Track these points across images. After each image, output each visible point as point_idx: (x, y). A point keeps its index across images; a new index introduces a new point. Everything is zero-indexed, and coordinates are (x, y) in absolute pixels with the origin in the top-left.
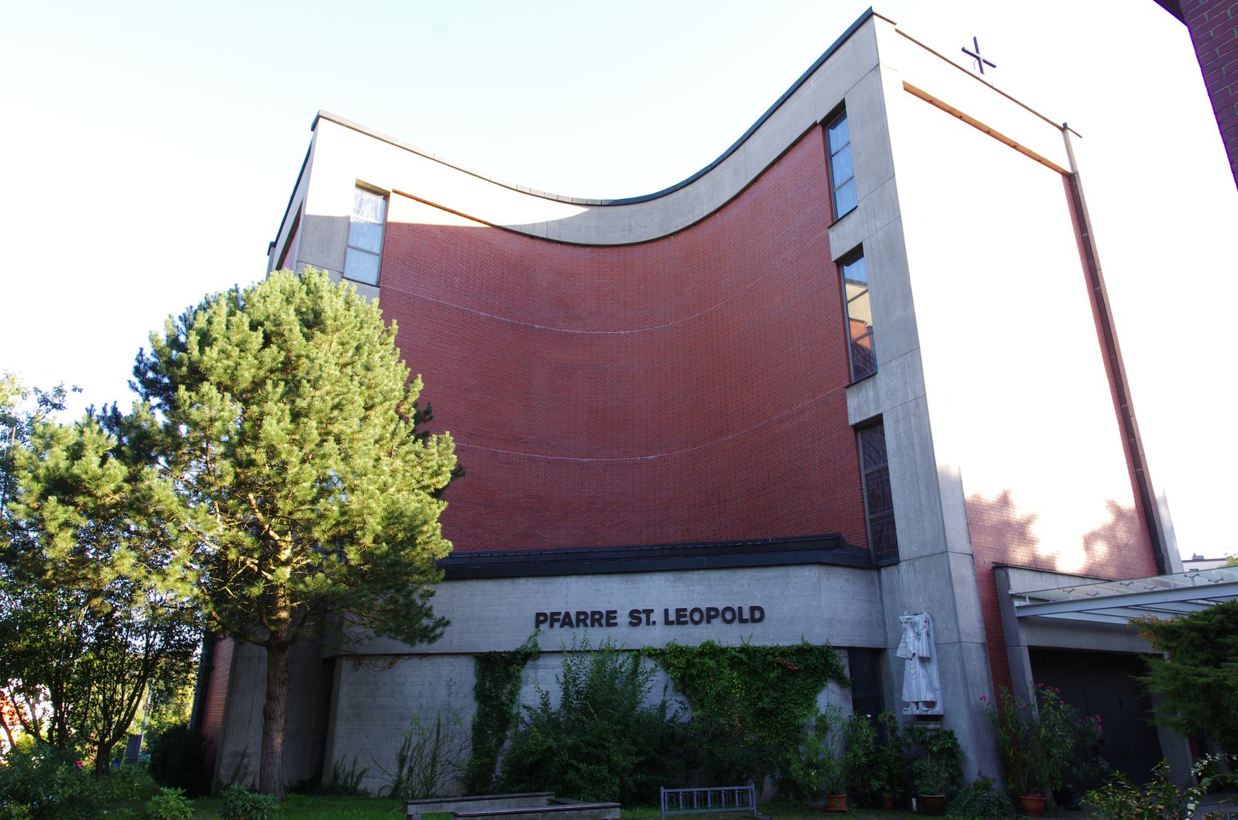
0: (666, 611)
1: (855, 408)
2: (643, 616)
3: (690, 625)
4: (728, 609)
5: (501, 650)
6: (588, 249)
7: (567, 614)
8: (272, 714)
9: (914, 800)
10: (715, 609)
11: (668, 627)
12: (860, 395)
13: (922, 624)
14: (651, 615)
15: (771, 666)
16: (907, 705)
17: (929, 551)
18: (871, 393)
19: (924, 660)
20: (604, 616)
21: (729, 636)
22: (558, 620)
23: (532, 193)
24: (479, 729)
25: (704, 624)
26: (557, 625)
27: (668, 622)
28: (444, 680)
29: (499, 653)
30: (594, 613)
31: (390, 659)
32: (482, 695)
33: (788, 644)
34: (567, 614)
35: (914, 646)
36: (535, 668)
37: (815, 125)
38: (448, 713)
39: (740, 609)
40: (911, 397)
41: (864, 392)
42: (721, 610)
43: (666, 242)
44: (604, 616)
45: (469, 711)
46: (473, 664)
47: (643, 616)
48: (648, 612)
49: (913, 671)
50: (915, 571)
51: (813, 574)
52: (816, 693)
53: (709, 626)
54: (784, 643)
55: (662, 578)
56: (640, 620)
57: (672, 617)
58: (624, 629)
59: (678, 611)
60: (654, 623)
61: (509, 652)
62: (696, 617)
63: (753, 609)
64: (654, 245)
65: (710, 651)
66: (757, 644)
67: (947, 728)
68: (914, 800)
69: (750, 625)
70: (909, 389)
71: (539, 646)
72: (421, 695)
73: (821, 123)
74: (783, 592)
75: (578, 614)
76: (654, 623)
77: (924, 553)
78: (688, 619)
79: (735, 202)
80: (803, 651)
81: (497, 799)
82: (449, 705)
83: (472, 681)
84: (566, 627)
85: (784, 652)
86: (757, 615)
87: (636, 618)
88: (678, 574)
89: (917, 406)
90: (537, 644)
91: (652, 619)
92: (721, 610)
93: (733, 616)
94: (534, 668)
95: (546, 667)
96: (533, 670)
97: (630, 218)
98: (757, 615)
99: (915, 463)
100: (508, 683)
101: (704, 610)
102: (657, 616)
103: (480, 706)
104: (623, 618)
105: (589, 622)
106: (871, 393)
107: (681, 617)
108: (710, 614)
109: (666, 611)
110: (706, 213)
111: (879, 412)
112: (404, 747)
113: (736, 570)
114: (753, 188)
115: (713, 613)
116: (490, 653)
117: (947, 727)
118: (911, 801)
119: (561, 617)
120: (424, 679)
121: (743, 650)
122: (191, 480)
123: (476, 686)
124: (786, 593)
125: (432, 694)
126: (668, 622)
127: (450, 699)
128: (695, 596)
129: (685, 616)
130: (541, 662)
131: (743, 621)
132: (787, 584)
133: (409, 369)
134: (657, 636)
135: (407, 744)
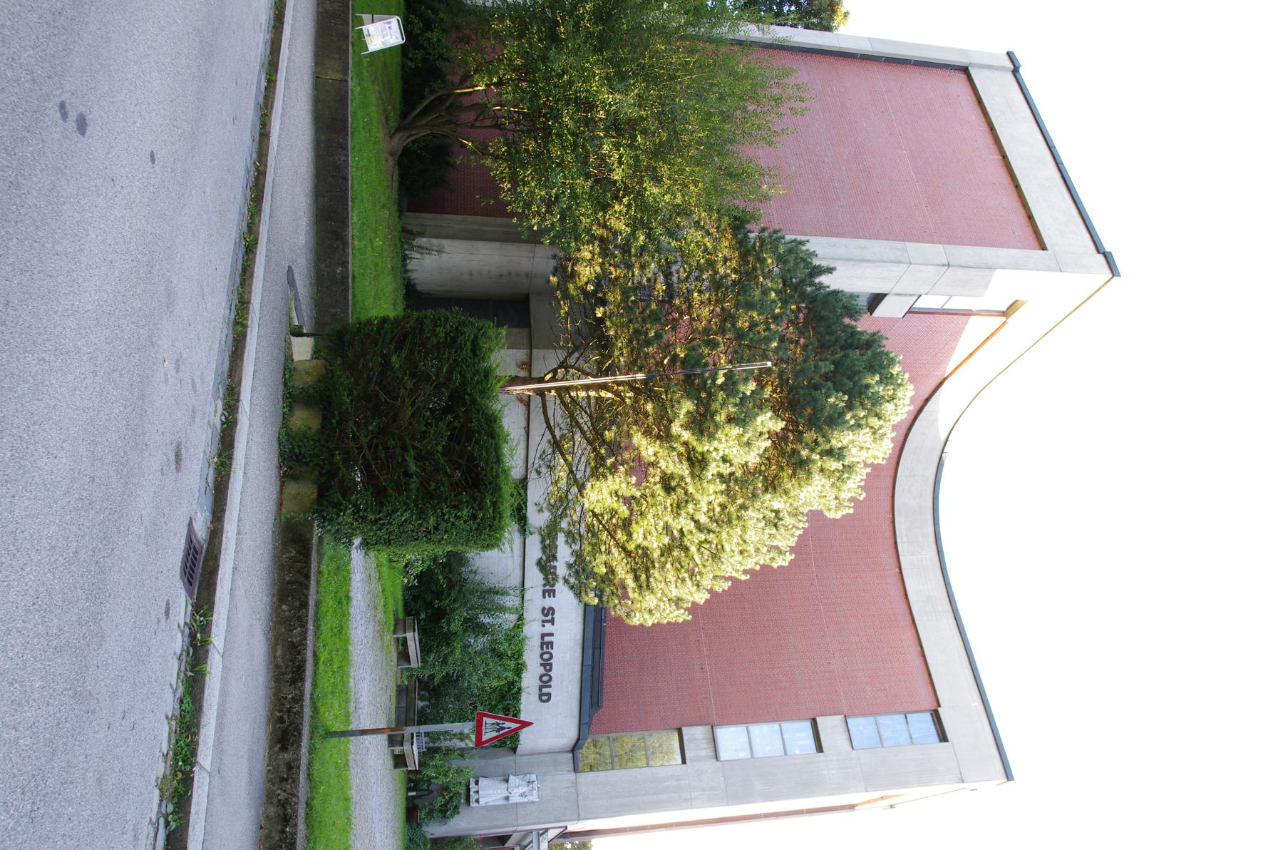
0: (552, 635)
1: (694, 734)
2: (549, 618)
10: (550, 670)
12: (704, 741)
16: (477, 783)
17: (581, 803)
19: (507, 798)
21: (529, 681)
27: (543, 636)
37: (939, 705)
39: (550, 686)
40: (693, 794)
41: (706, 746)
43: (888, 509)
46: (518, 477)
47: (549, 618)
48: (552, 621)
56: (546, 615)
57: (547, 639)
59: (551, 643)
60: (543, 626)
63: (549, 695)
69: (538, 692)
71: (531, 536)
76: (543, 626)
77: (580, 798)
86: (545, 697)
87: (548, 613)
93: (545, 681)
98: (544, 698)
99: (645, 795)
107: (546, 645)
108: (547, 665)
109: (552, 635)
115: (548, 668)
117: (462, 809)
126: (543, 636)
131: (541, 688)
134: (533, 629)
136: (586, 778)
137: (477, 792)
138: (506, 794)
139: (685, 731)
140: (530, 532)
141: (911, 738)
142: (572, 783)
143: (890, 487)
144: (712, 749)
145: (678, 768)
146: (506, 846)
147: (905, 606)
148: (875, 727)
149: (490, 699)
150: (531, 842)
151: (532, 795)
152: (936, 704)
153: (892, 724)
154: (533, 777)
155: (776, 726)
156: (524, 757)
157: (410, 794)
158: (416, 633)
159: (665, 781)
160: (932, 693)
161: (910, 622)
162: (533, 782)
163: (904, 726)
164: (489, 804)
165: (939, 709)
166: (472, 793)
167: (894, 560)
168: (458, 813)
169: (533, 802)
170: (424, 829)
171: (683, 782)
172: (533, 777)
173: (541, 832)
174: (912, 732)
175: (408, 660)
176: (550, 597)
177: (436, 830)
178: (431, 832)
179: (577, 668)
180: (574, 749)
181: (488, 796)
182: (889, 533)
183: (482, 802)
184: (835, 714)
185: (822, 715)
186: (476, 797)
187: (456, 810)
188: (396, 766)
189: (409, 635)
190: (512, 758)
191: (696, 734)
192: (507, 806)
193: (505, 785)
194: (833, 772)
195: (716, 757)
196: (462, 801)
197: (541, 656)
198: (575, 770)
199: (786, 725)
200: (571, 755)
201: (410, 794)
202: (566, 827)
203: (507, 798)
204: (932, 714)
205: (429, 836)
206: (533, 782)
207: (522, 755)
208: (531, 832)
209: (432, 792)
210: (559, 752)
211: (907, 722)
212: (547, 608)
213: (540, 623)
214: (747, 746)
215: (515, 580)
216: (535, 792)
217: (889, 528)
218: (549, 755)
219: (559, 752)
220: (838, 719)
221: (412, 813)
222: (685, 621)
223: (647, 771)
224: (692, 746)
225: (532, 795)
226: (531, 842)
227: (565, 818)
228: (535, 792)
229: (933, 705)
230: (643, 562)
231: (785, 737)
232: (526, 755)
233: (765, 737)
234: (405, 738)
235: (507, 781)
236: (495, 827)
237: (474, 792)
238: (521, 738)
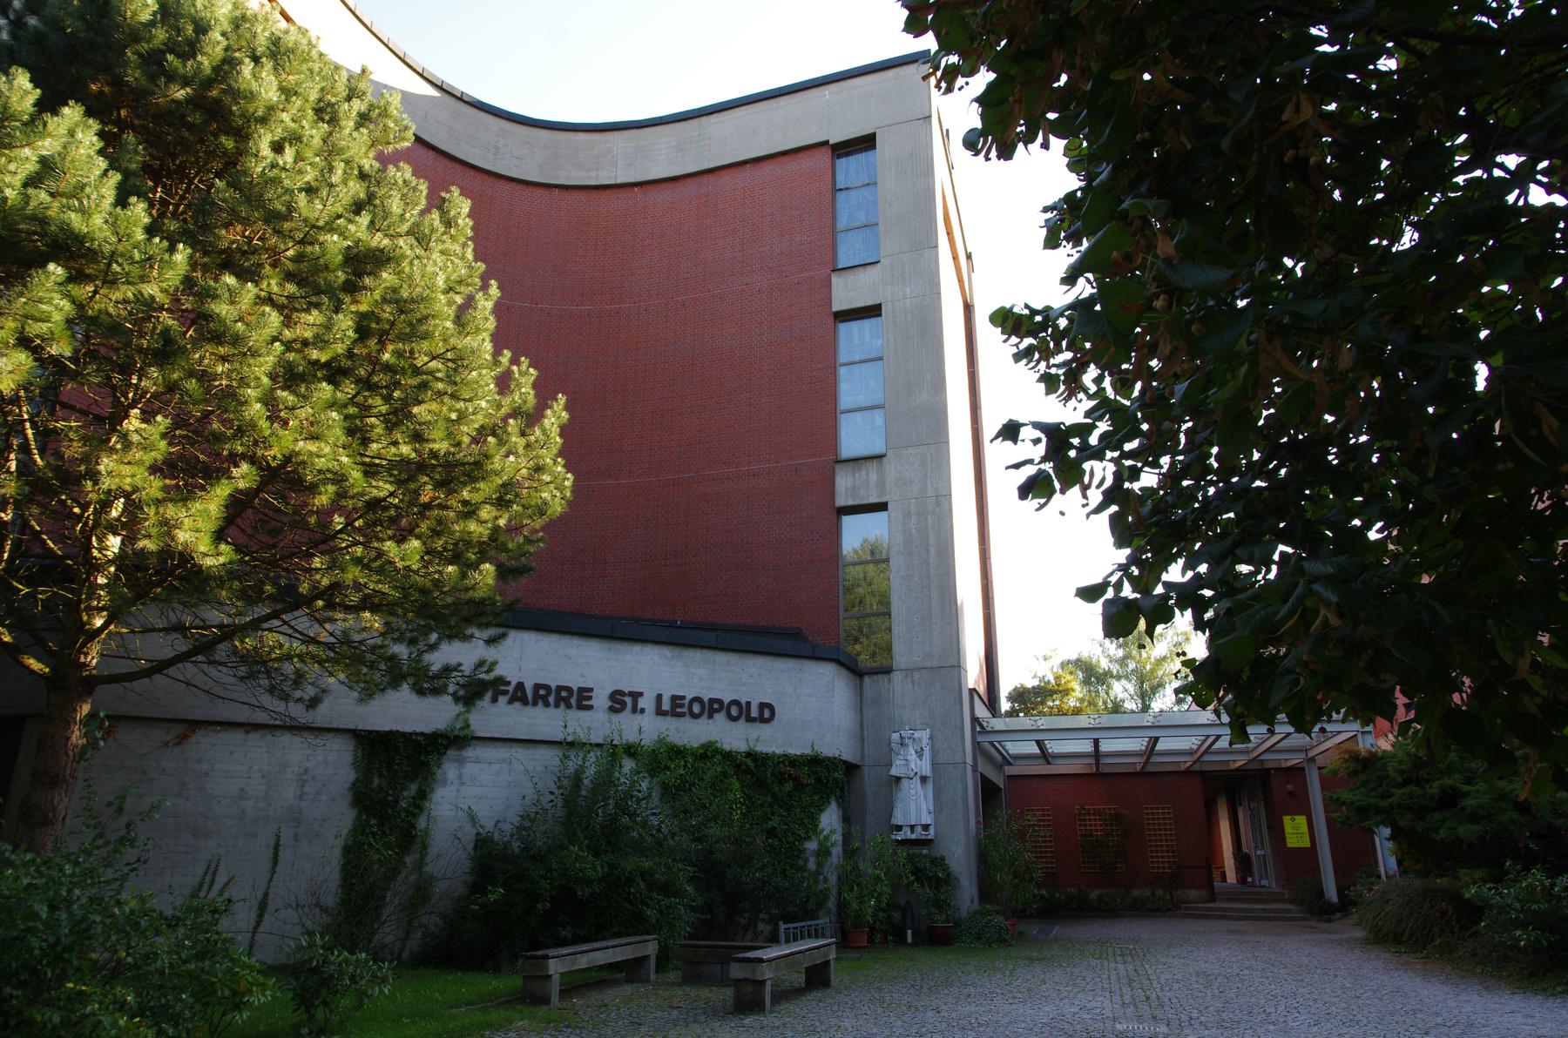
0: (659, 697)
1: (847, 489)
2: (628, 700)
3: (687, 719)
4: (735, 702)
5: (407, 728)
6: (431, 154)
7: (520, 686)
8: (51, 815)
9: (909, 932)
10: (720, 702)
11: (660, 718)
12: (857, 475)
13: (925, 741)
14: (640, 699)
15: (781, 778)
16: (899, 828)
17: (936, 663)
18: (873, 477)
19: (924, 779)
20: (575, 693)
21: (734, 737)
22: (506, 692)
23: (374, 30)
24: (353, 853)
25: (704, 720)
26: (503, 699)
27: (660, 712)
28: (293, 772)
29: (404, 735)
30: (560, 688)
31: (179, 729)
32: (363, 798)
33: (798, 753)
34: (520, 686)
35: (916, 764)
36: (461, 762)
37: (826, 143)
38: (297, 827)
39: (748, 704)
40: (930, 492)
41: (863, 473)
42: (726, 703)
43: (545, 193)
44: (575, 693)
45: (341, 819)
46: (352, 747)
47: (628, 700)
48: (636, 696)
49: (913, 792)
50: (913, 682)
51: (827, 673)
52: (821, 811)
53: (710, 721)
54: (795, 751)
55: (656, 651)
56: (624, 705)
57: (666, 706)
58: (601, 715)
59: (674, 698)
60: (643, 711)
61: (422, 734)
62: (696, 708)
63: (762, 706)
64: (528, 190)
65: (709, 752)
66: (765, 750)
67: (937, 853)
68: (909, 932)
69: (757, 725)
70: (929, 484)
71: (473, 727)
72: (243, 794)
73: (832, 145)
74: (795, 689)
75: (537, 687)
76: (643, 711)
77: (928, 664)
78: (685, 710)
79: (669, 185)
80: (815, 761)
81: (597, 950)
82: (300, 813)
83: (348, 775)
84: (517, 705)
85: (792, 761)
86: (766, 713)
87: (621, 701)
88: (676, 651)
89: (938, 504)
90: (468, 726)
91: (640, 705)
92: (726, 703)
93: (739, 711)
94: (457, 761)
95: (477, 761)
96: (456, 764)
97: (497, 136)
98: (767, 714)
99: (928, 564)
100: (412, 781)
101: (706, 700)
102: (646, 702)
103: (358, 818)
104: (600, 700)
105: (551, 699)
106: (873, 477)
107: (677, 707)
108: (712, 707)
109: (659, 697)
110: (620, 180)
111: (884, 500)
112: (201, 885)
113: (746, 655)
114: (706, 178)
115: (716, 706)
116: (391, 732)
117: (937, 852)
118: (906, 933)
119: (511, 688)
120: (251, 767)
121: (750, 754)
122: (1023, 346)
123: (354, 784)
124: (799, 691)
125: (266, 792)
126: (660, 712)
127: (303, 804)
128: (695, 681)
129: (682, 706)
130: (470, 752)
131: (750, 719)
132: (801, 680)
133: (1084, 288)
134: (644, 728)
135: (208, 879)
136: (902, 655)
137: (912, 827)
138: (917, 781)
139: (841, 501)
140: (462, 729)
141: (869, 184)
142: (906, 676)
143: (510, 185)
144: (869, 464)
145: (893, 514)
146: (1002, 786)
147: (690, 182)
148: (851, 233)
149: (762, 806)
150: (991, 743)
151: (920, 740)
152: (824, 149)
153: (848, 209)
154: (895, 737)
155: (843, 371)
156: (866, 752)
157: (910, 940)
158: (551, 952)
159: (910, 534)
160: (810, 153)
161: (711, 177)
162: (902, 738)
163: (852, 193)
164: (931, 808)
165: (831, 142)
166: (913, 837)
167: (622, 194)
168: (943, 859)
169: (931, 738)
170: (964, 914)
171: (912, 508)
172: (895, 737)
173: (978, 729)
174: (861, 184)
175: (640, 962)
176: (590, 698)
177: (966, 895)
178: (968, 902)
179: (721, 657)
180: (857, 672)
181: (918, 810)
182: (582, 196)
183: (927, 819)
184: (830, 281)
185: (830, 304)
186: (919, 829)
187: (939, 862)
188: (826, 984)
189: (555, 967)
190: (866, 771)
191: (847, 487)
192: (936, 780)
193: (905, 782)
194: (908, 292)
195: (880, 457)
196: (925, 852)
197: (695, 716)
198: (888, 671)
199: (843, 357)
200: (866, 679)
201: (910, 940)
202: (973, 691)
203: (924, 779)
204: (839, 157)
205: (976, 906)
206: (902, 738)
207: (863, 756)
208: (977, 745)
209: (908, 902)
210: (861, 697)
211: (846, 189)
212: (610, 704)
213: (638, 718)
214: (867, 413)
215: (550, 757)
216: (917, 735)
217: (575, 195)
218: (865, 709)
219: (861, 697)
220: (837, 281)
221: (938, 938)
222: (567, 408)
223: (894, 563)
224: (862, 492)
225: (920, 740)
226: (991, 743)
227: (957, 689)
228: (917, 735)
229: (824, 156)
230: (536, 531)
231: (857, 359)
232: (863, 750)
233: (853, 388)
234: (749, 976)
235: (898, 779)
236: (965, 800)
237: (912, 832)
238: (830, 755)
